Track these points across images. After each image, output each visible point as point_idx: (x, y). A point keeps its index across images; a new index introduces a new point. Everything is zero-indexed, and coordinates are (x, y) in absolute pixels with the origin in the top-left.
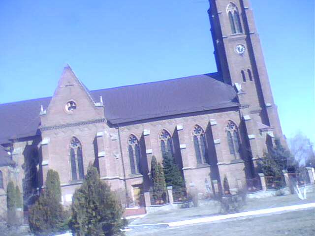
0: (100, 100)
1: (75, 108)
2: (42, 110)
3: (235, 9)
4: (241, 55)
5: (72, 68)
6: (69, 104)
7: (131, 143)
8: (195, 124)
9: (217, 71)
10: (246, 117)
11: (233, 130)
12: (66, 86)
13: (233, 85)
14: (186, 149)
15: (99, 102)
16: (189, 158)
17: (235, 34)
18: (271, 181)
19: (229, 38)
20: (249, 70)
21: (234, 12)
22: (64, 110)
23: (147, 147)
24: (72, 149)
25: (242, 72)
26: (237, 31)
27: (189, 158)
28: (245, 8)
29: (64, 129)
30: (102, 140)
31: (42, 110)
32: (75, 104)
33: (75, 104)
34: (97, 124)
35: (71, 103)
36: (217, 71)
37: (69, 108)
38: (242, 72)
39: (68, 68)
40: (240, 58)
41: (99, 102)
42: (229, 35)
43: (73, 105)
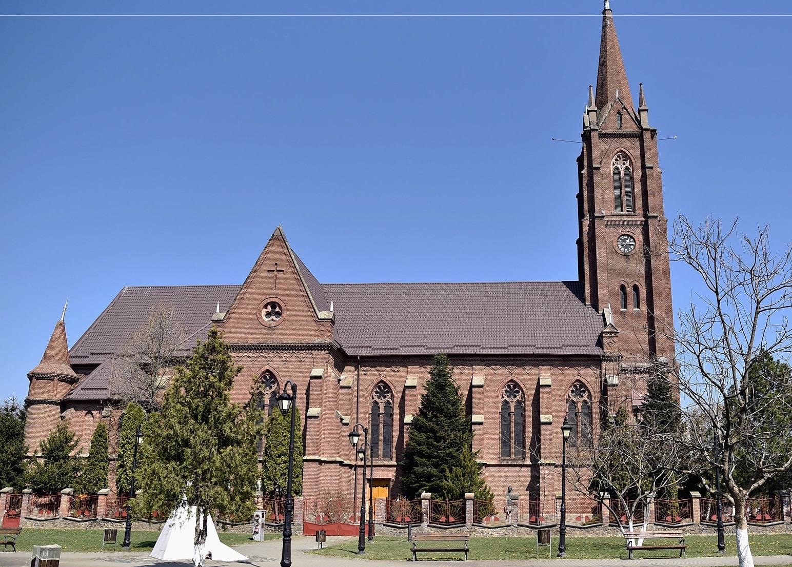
0: (330, 307)
1: (278, 314)
2: (218, 311)
3: (627, 164)
4: (627, 255)
5: (287, 238)
6: (269, 307)
7: (379, 397)
8: (267, 367)
9: (577, 280)
10: (613, 380)
11: (581, 400)
12: (268, 271)
13: (601, 312)
14: (484, 426)
15: (328, 309)
16: (487, 443)
17: (620, 213)
18: (202, 504)
19: (606, 219)
20: (636, 288)
21: (623, 169)
22: (258, 318)
23: (541, 412)
24: (376, 402)
25: (623, 288)
26: (625, 208)
27: (486, 443)
28: (647, 165)
29: (251, 354)
30: (321, 386)
31: (218, 311)
32: (280, 308)
33: (280, 308)
34: (315, 353)
35: (274, 305)
36: (577, 280)
37: (268, 314)
38: (623, 288)
39: (278, 237)
40: (622, 261)
41: (328, 309)
42: (608, 213)
43: (277, 309)
